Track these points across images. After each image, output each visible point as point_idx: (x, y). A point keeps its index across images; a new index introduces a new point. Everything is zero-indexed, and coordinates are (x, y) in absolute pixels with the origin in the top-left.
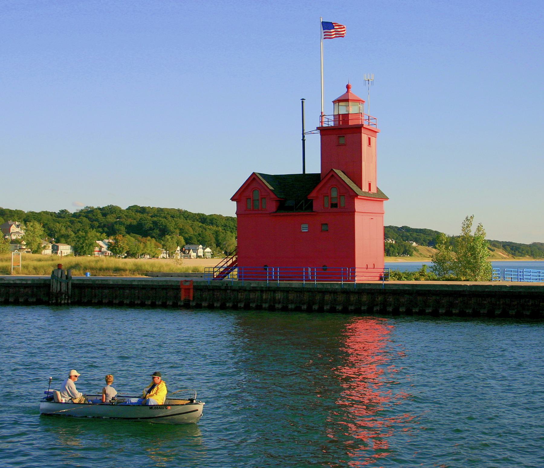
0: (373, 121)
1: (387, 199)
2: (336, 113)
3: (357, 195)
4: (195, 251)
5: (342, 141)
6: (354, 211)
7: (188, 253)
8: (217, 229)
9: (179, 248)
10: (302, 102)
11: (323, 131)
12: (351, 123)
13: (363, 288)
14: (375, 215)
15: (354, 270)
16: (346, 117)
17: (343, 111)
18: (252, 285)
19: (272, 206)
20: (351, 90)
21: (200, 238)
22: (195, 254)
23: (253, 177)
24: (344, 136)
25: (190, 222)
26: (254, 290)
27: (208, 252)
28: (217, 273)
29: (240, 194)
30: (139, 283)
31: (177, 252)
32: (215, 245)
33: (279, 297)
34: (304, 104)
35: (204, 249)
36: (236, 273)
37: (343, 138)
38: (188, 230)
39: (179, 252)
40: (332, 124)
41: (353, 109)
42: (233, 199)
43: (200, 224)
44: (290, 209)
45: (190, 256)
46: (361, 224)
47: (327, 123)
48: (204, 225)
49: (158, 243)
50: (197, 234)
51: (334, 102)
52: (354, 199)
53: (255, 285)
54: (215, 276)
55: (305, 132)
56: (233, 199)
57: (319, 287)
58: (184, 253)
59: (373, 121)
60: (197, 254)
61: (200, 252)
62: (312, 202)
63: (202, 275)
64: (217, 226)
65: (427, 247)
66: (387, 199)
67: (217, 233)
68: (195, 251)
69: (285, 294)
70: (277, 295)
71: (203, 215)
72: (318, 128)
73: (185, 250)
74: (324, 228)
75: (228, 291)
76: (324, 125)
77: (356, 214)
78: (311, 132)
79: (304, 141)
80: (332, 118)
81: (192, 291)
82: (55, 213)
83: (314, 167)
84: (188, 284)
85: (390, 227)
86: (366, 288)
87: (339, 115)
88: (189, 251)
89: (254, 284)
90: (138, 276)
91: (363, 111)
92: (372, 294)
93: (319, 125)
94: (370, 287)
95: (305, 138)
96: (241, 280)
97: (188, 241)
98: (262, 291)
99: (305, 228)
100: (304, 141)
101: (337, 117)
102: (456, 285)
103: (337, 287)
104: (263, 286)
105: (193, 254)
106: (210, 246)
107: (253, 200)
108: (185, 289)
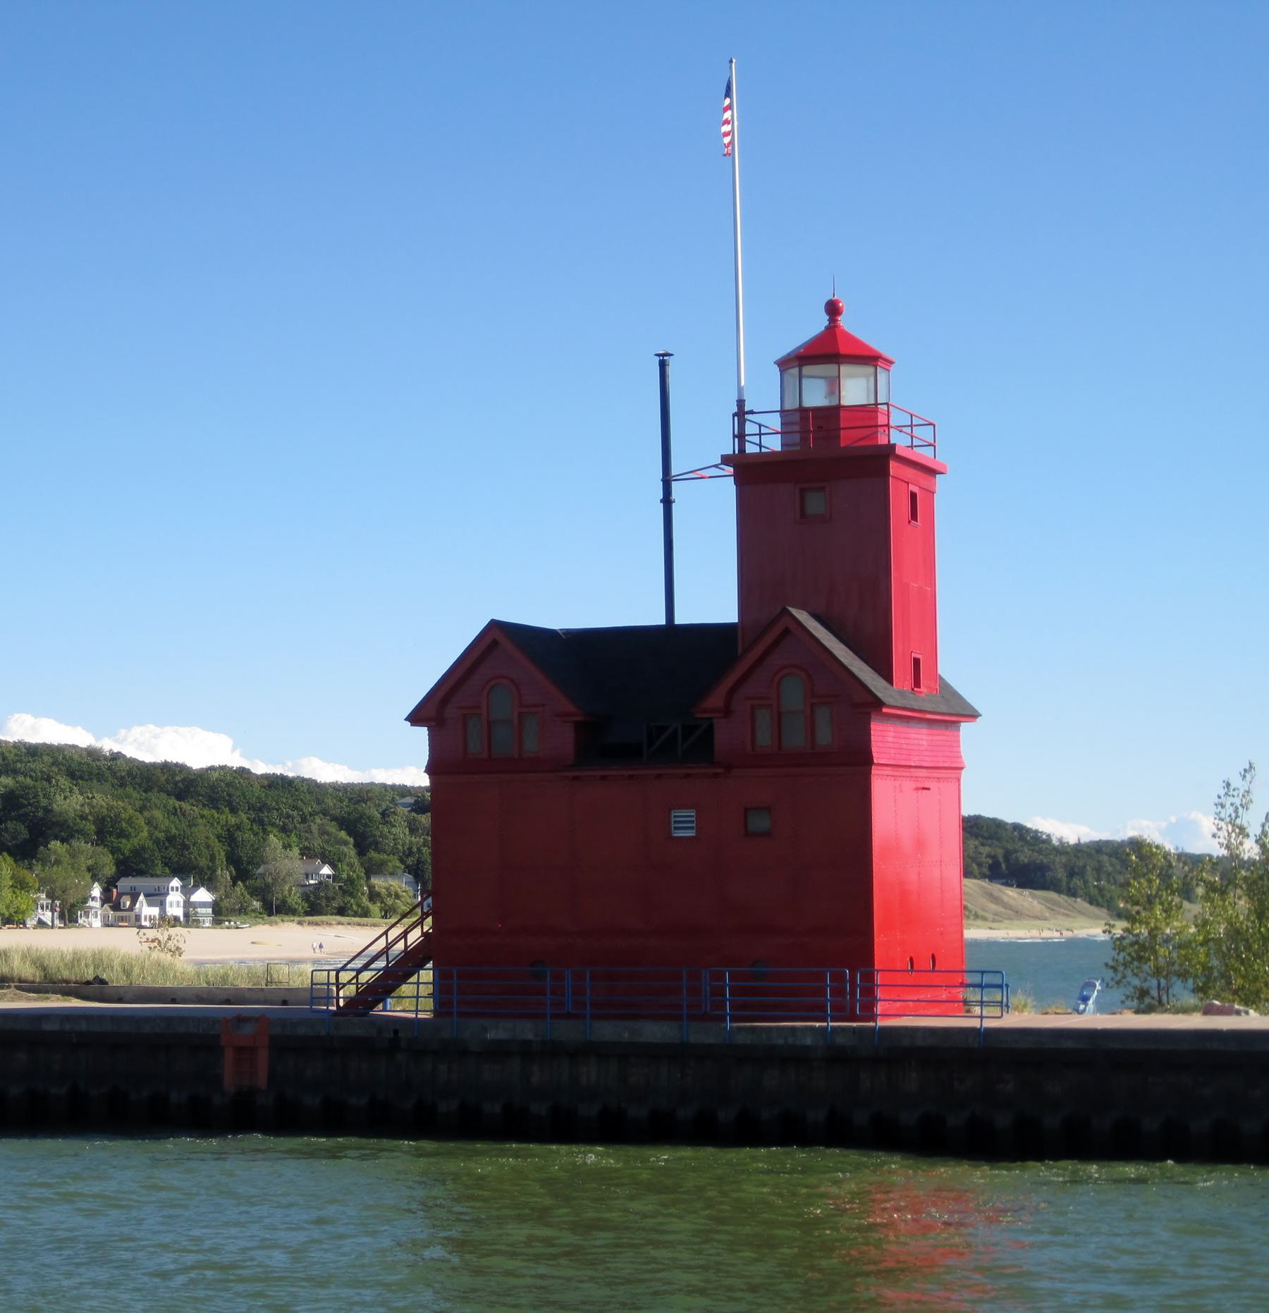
0: (924, 433)
1: (973, 715)
2: (791, 404)
3: (875, 704)
4: (157, 897)
5: (816, 504)
6: (865, 759)
7: (131, 909)
8: (233, 820)
9: (96, 891)
10: (663, 366)
11: (750, 472)
12: (847, 439)
14: (936, 774)
15: (869, 977)
16: (830, 416)
17: (815, 396)
18: (490, 1036)
19: (564, 740)
20: (844, 321)
21: (171, 852)
22: (155, 911)
23: (488, 641)
24: (823, 489)
25: (135, 795)
26: (498, 1052)
27: (203, 905)
28: (350, 990)
29: (445, 701)
30: (67, 1027)
31: (91, 903)
32: (224, 875)
34: (670, 370)
35: (187, 891)
36: (426, 990)
37: (828, 500)
38: (130, 821)
39: (97, 904)
40: (774, 444)
41: (855, 389)
42: (415, 718)
43: (173, 802)
44: (626, 753)
45: (138, 918)
46: (893, 807)
47: (756, 439)
48: (185, 806)
49: (25, 873)
50: (161, 836)
51: (784, 364)
52: (869, 714)
53: (502, 1035)
54: (341, 1003)
55: (674, 471)
56: (415, 718)
58: (116, 907)
59: (924, 433)
60: (163, 910)
61: (175, 903)
62: (711, 727)
63: (287, 997)
64: (234, 811)
65: (985, 884)
66: (973, 715)
67: (229, 838)
68: (157, 897)
71: (181, 768)
72: (726, 460)
73: (120, 895)
74: (760, 823)
76: (751, 449)
77: (874, 771)
78: (696, 475)
79: (667, 501)
80: (775, 422)
81: (263, 1057)
82: (1211, 857)
83: (712, 598)
84: (248, 1029)
85: (977, 819)
87: (803, 411)
88: (134, 900)
89: (498, 1032)
90: (55, 1002)
91: (912, 399)
93: (729, 448)
95: (674, 496)
96: (450, 1014)
97: (132, 865)
99: (684, 824)
100: (667, 501)
101: (797, 417)
103: (808, 1041)
105: (148, 911)
106: (207, 880)
107: (489, 724)
108: (239, 1050)
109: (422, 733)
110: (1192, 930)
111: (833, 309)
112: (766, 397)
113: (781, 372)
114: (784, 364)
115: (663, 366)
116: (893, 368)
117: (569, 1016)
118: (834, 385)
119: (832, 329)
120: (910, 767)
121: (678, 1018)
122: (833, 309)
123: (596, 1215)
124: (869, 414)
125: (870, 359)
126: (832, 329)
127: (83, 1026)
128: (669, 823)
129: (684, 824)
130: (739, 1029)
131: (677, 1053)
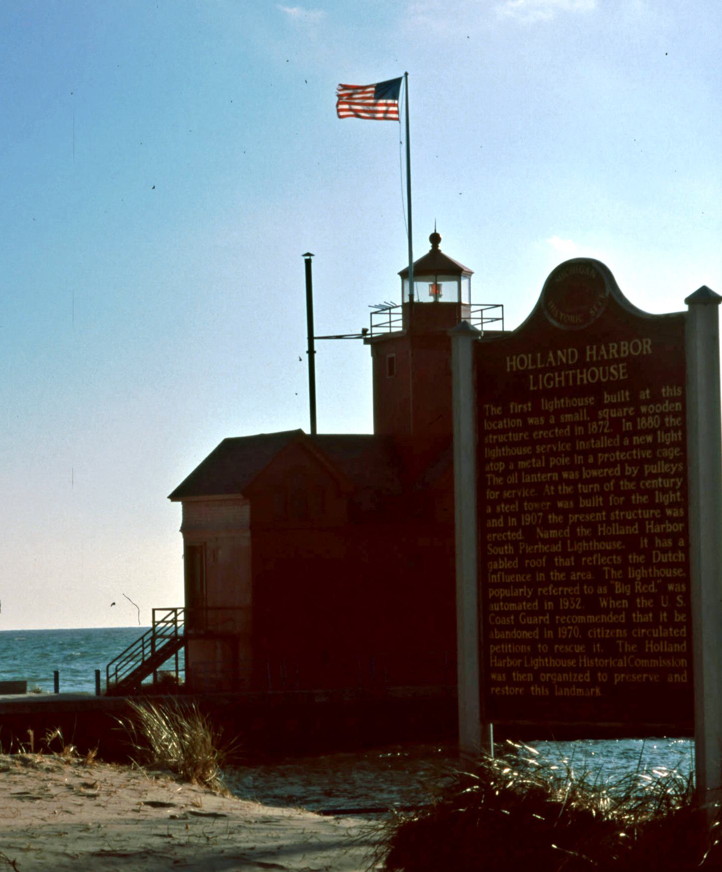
10: (308, 263)
11: (380, 345)
17: (423, 293)
20: (441, 247)
41: (448, 293)
42: (174, 497)
56: (174, 497)
79: (311, 352)
95: (316, 349)
100: (311, 352)
109: (179, 505)
110: (605, 803)
111: (435, 239)
114: (404, 274)
115: (308, 263)
116: (473, 276)
118: (436, 291)
119: (435, 252)
122: (435, 239)
123: (13, 840)
124: (455, 308)
125: (455, 272)
126: (435, 252)
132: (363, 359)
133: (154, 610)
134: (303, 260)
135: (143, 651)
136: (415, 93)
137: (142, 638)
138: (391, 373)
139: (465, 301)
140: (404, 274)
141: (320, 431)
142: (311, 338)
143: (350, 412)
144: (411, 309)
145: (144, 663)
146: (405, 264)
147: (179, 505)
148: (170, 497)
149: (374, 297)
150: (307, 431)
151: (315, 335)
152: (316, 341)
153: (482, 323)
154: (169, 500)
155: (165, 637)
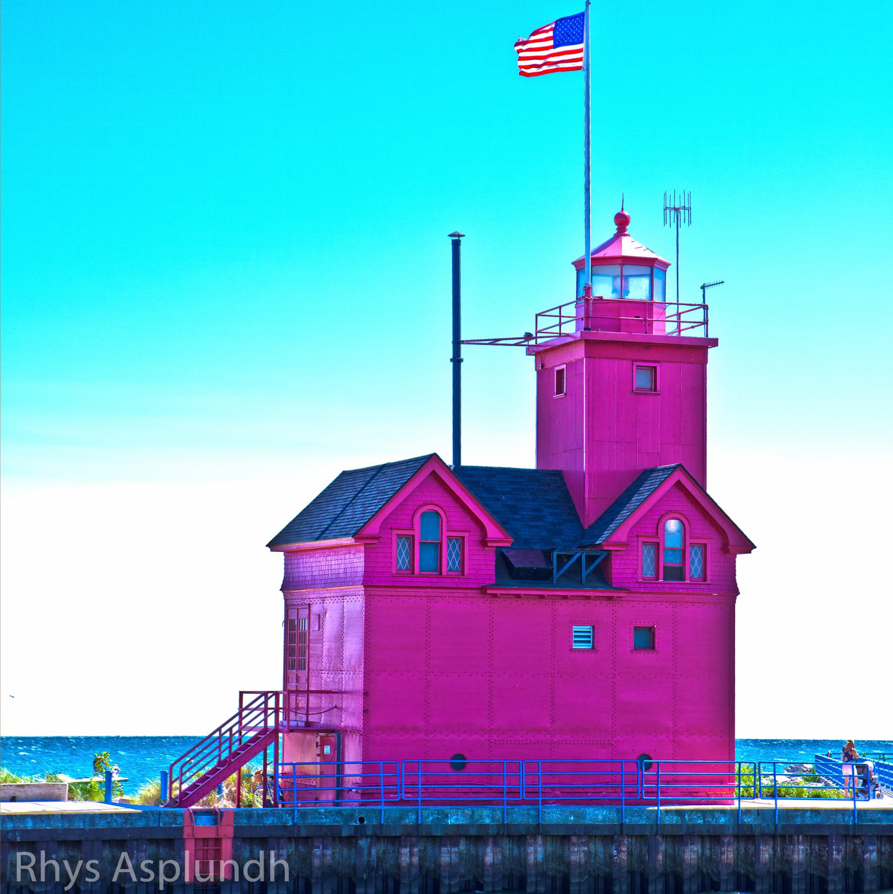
1: (748, 546)
10: (456, 245)
11: (543, 353)
13: (798, 821)
18: (451, 821)
26: (453, 836)
33: (540, 856)
37: (630, 375)
42: (274, 545)
53: (462, 821)
55: (464, 337)
56: (274, 545)
57: (667, 820)
66: (748, 546)
69: (302, 849)
70: (531, 849)
75: (363, 843)
79: (457, 361)
86: (808, 821)
89: (455, 818)
92: (823, 838)
94: (818, 820)
98: (396, 840)
99: (581, 637)
100: (457, 361)
102: (796, 810)
103: (722, 820)
104: (487, 821)
109: (280, 556)
112: (564, 290)
113: (577, 270)
114: (579, 265)
115: (456, 245)
117: (523, 802)
120: (431, 588)
121: (618, 802)
127: (30, 825)
128: (571, 637)
129: (581, 637)
130: (667, 812)
131: (609, 836)
132: (524, 371)
133: (241, 693)
134: (450, 239)
135: (219, 747)
136: (594, 27)
137: (219, 729)
138: (559, 391)
139: (657, 299)
140: (579, 265)
141: (465, 462)
142: (457, 343)
143: (505, 440)
144: (592, 310)
145: (220, 763)
146: (579, 253)
147: (280, 556)
148: (679, 481)
149: (534, 289)
150: (448, 460)
151: (463, 338)
152: (463, 346)
153: (560, 324)
154: (268, 549)
155: (252, 729)
